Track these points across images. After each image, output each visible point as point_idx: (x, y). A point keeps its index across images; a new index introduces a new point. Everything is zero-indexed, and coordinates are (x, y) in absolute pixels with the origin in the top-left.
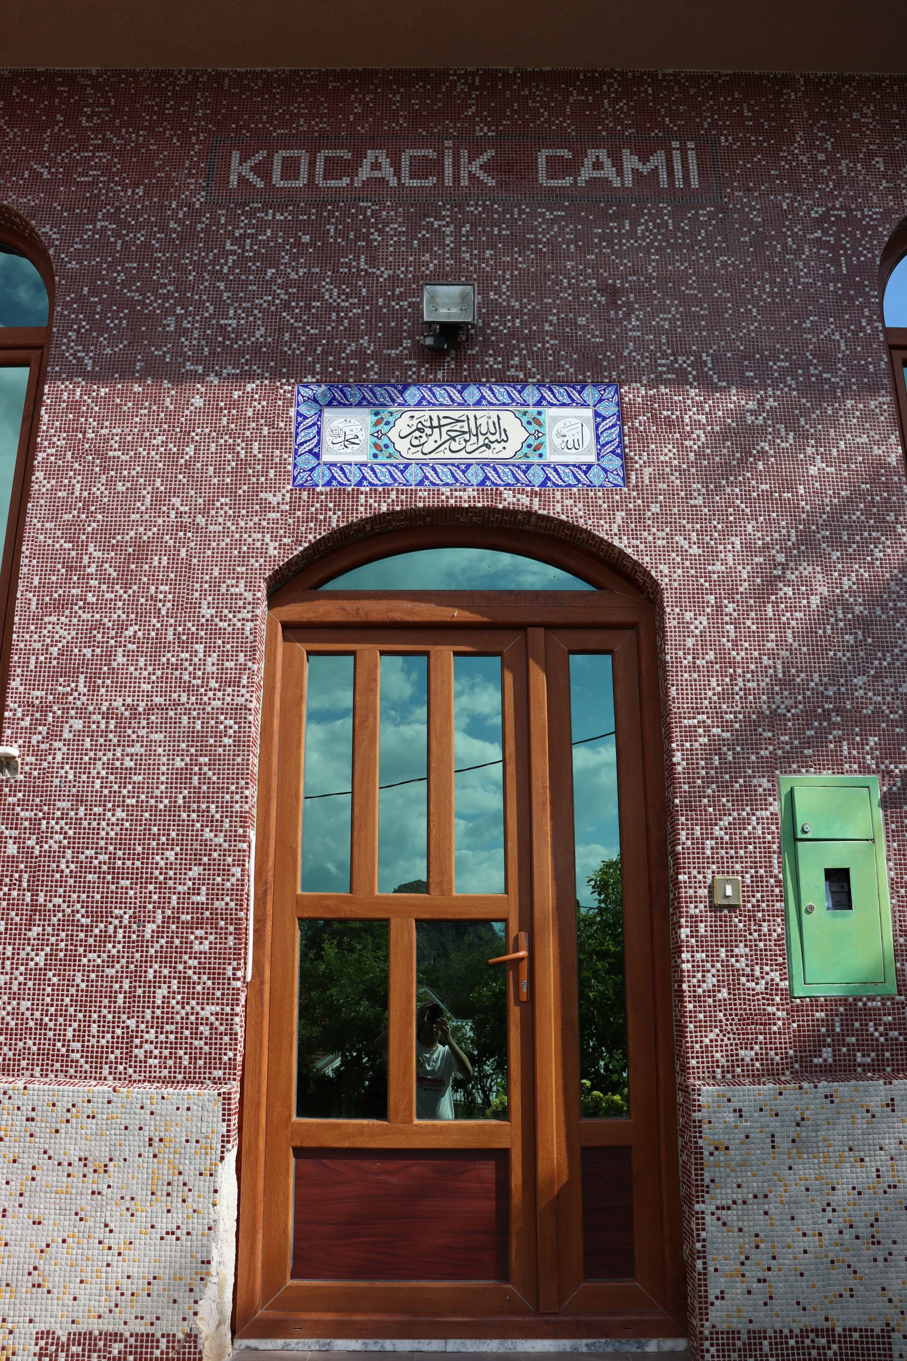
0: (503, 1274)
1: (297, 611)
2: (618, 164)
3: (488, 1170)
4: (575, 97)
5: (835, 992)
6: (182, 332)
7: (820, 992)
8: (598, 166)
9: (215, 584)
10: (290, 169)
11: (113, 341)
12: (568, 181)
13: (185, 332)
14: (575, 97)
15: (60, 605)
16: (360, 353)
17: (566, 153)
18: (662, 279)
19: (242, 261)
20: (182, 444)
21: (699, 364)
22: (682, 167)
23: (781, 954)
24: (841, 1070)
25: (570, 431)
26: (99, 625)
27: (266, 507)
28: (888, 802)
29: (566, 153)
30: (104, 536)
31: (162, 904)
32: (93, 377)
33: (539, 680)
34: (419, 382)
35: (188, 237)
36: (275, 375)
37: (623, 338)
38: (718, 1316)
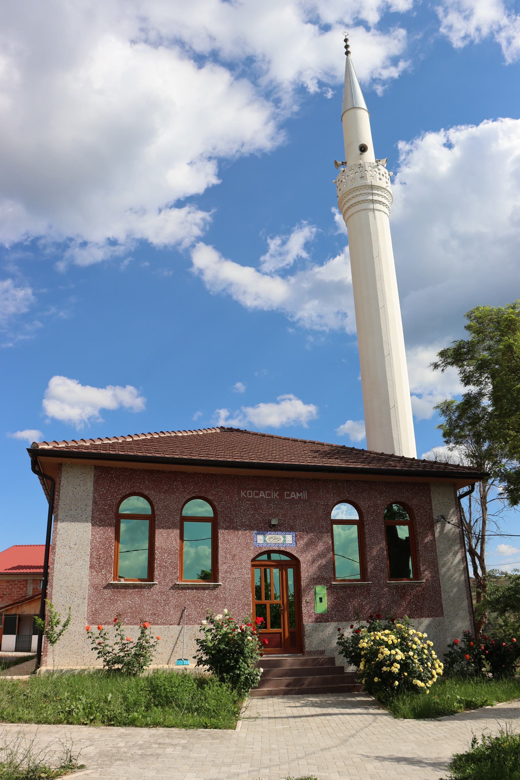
0: (281, 647)
1: (254, 563)
2: (296, 495)
3: (279, 635)
4: (290, 482)
5: (320, 612)
6: (237, 522)
7: (319, 613)
8: (293, 495)
9: (245, 560)
10: (250, 495)
11: (227, 523)
12: (289, 498)
13: (237, 522)
14: (290, 482)
15: (225, 563)
16: (261, 526)
17: (288, 493)
18: (302, 515)
19: (244, 510)
20: (239, 540)
21: (306, 528)
22: (304, 495)
23: (314, 608)
24: (321, 622)
25: (289, 538)
26: (230, 566)
27: (251, 550)
28: (327, 589)
29: (288, 493)
30: (230, 553)
31: (241, 603)
32: (226, 529)
33: (284, 573)
34: (270, 531)
35: (236, 505)
36: (250, 530)
37: (296, 524)
38: (307, 649)
